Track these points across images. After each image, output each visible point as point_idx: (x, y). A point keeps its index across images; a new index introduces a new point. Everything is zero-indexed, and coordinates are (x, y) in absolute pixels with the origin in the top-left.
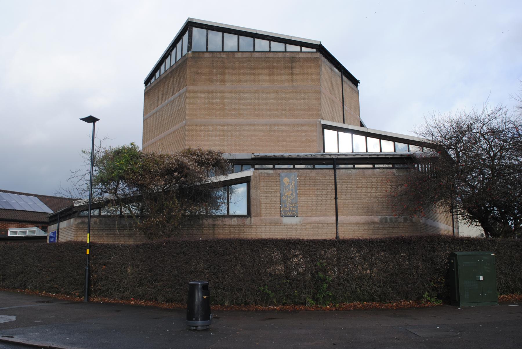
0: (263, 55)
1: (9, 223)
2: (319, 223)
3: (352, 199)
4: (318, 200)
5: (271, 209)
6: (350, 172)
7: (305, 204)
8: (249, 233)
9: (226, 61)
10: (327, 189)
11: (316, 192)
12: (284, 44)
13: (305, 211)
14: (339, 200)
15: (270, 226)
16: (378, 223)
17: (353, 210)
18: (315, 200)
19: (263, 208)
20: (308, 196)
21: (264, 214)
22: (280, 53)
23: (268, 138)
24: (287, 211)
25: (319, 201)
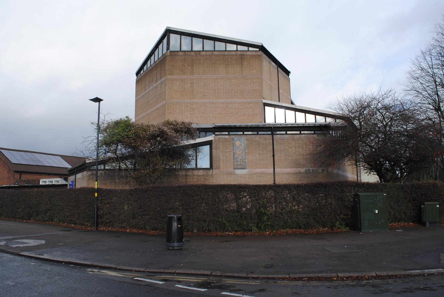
1: (41, 176)
2: (262, 174)
4: (260, 157)
6: (284, 137)
7: (251, 160)
8: (212, 181)
11: (259, 151)
13: (252, 165)
14: (276, 157)
16: (303, 173)
17: (286, 164)
18: (258, 157)
21: (222, 167)
23: (225, 113)
24: (238, 165)
25: (262, 157)
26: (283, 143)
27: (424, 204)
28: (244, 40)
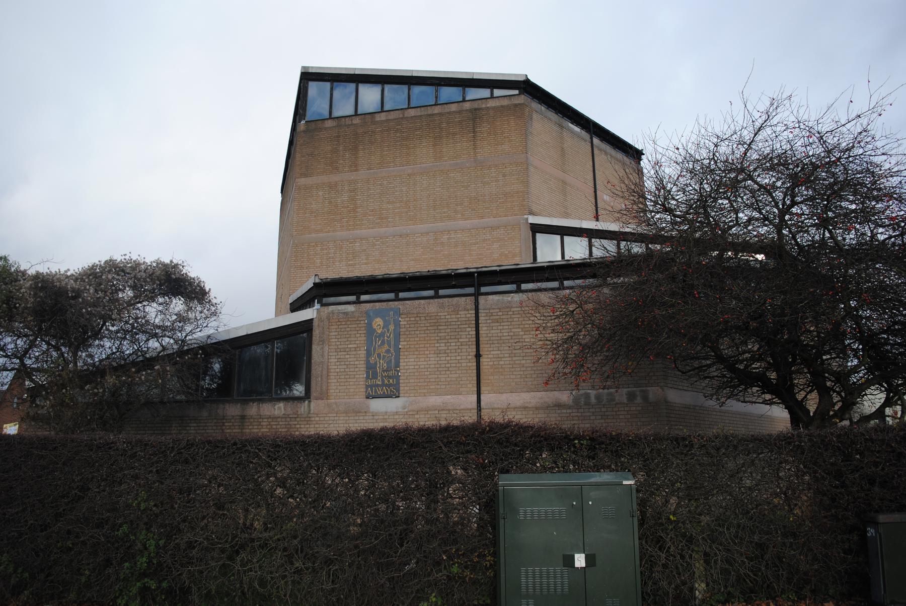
3: (513, 355)
4: (439, 362)
6: (509, 299)
9: (360, 131)
10: (459, 337)
12: (461, 88)
14: (485, 360)
15: (346, 418)
16: (569, 407)
17: (515, 380)
18: (434, 362)
20: (421, 353)
23: (431, 258)
24: (378, 386)
25: (444, 362)
26: (507, 317)
27: (875, 524)
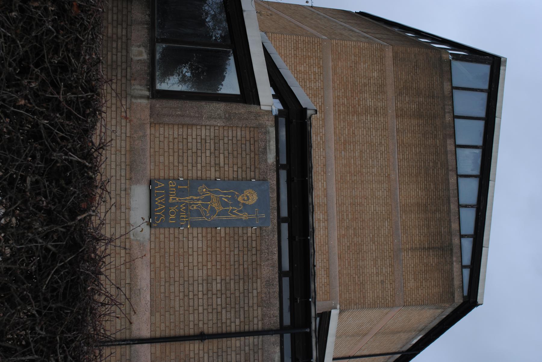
0: (452, 192)
2: (131, 290)
5: (171, 153)
7: (186, 247)
10: (228, 309)
13: (167, 250)
14: (197, 346)
18: (196, 275)
19: (176, 132)
20: (209, 257)
21: (157, 135)
22: (457, 225)
24: (167, 198)
25: (196, 289)
28: (487, 255)
